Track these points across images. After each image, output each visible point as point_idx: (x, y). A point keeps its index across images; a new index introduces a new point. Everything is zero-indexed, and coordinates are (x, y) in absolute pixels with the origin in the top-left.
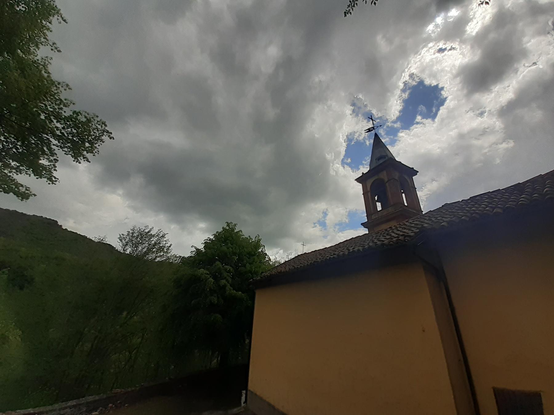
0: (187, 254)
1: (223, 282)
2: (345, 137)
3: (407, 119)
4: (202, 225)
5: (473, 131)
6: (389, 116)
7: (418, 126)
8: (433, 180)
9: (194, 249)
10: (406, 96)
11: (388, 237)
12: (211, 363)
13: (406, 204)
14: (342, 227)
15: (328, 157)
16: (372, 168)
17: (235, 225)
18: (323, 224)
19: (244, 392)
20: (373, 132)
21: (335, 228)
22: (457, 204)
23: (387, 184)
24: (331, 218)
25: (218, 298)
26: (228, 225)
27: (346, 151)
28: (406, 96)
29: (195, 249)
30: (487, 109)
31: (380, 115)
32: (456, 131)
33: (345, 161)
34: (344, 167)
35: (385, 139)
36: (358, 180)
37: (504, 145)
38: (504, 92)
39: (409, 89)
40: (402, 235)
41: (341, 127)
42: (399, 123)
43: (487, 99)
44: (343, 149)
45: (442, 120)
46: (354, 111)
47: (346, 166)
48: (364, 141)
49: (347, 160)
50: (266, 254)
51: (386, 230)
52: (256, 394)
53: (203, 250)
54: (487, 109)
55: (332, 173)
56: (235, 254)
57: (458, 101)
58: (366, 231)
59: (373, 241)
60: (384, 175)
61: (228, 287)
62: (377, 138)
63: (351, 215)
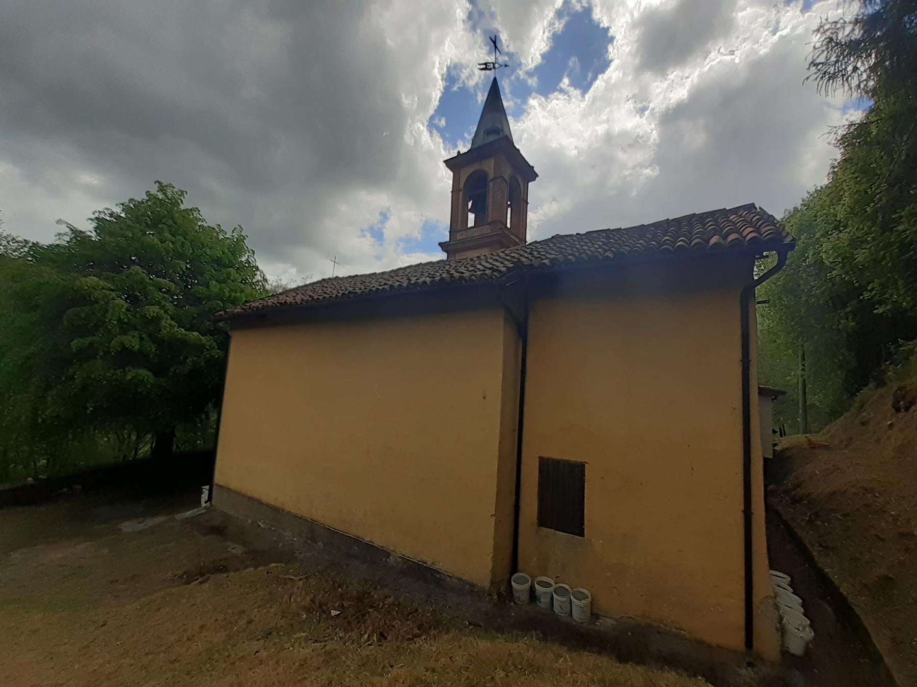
0: (47, 238)
1: (153, 310)
2: (445, 69)
3: (548, 78)
4: (90, 178)
5: (624, 134)
6: (526, 59)
7: (561, 96)
8: (554, 199)
9: (64, 229)
10: (559, 26)
11: (471, 269)
12: (136, 452)
13: (509, 226)
14: (409, 244)
15: (406, 102)
16: (475, 146)
17: (182, 193)
18: (378, 235)
19: (207, 487)
20: (491, 74)
21: (398, 245)
22: (569, 239)
23: (491, 184)
24: (392, 224)
25: (141, 339)
26: (162, 189)
27: (441, 100)
28: (561, 26)
29: (68, 230)
30: (651, 105)
31: (512, 49)
32: (605, 126)
33: (436, 121)
34: (431, 132)
35: (508, 101)
36: (449, 163)
37: (648, 172)
38: (677, 86)
39: (568, 14)
40: (490, 269)
41: (440, 42)
42: (535, 79)
43: (657, 87)
44: (436, 95)
45: (595, 99)
46: (470, 16)
47: (435, 132)
48: (475, 91)
49: (440, 120)
50: (257, 269)
51: (472, 260)
52: (229, 489)
53: (93, 234)
54: (651, 105)
55: (408, 139)
56: (181, 256)
57: (624, 74)
58: (443, 256)
59: (448, 272)
60: (489, 166)
61: (166, 322)
62: (494, 92)
63: (428, 227)
